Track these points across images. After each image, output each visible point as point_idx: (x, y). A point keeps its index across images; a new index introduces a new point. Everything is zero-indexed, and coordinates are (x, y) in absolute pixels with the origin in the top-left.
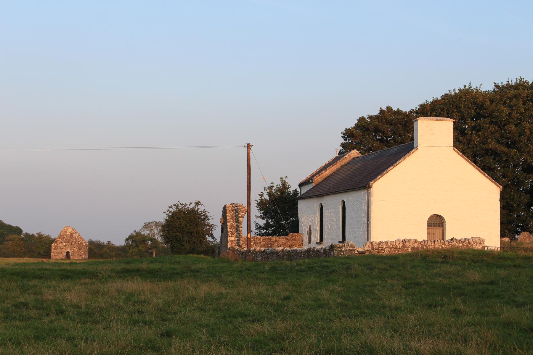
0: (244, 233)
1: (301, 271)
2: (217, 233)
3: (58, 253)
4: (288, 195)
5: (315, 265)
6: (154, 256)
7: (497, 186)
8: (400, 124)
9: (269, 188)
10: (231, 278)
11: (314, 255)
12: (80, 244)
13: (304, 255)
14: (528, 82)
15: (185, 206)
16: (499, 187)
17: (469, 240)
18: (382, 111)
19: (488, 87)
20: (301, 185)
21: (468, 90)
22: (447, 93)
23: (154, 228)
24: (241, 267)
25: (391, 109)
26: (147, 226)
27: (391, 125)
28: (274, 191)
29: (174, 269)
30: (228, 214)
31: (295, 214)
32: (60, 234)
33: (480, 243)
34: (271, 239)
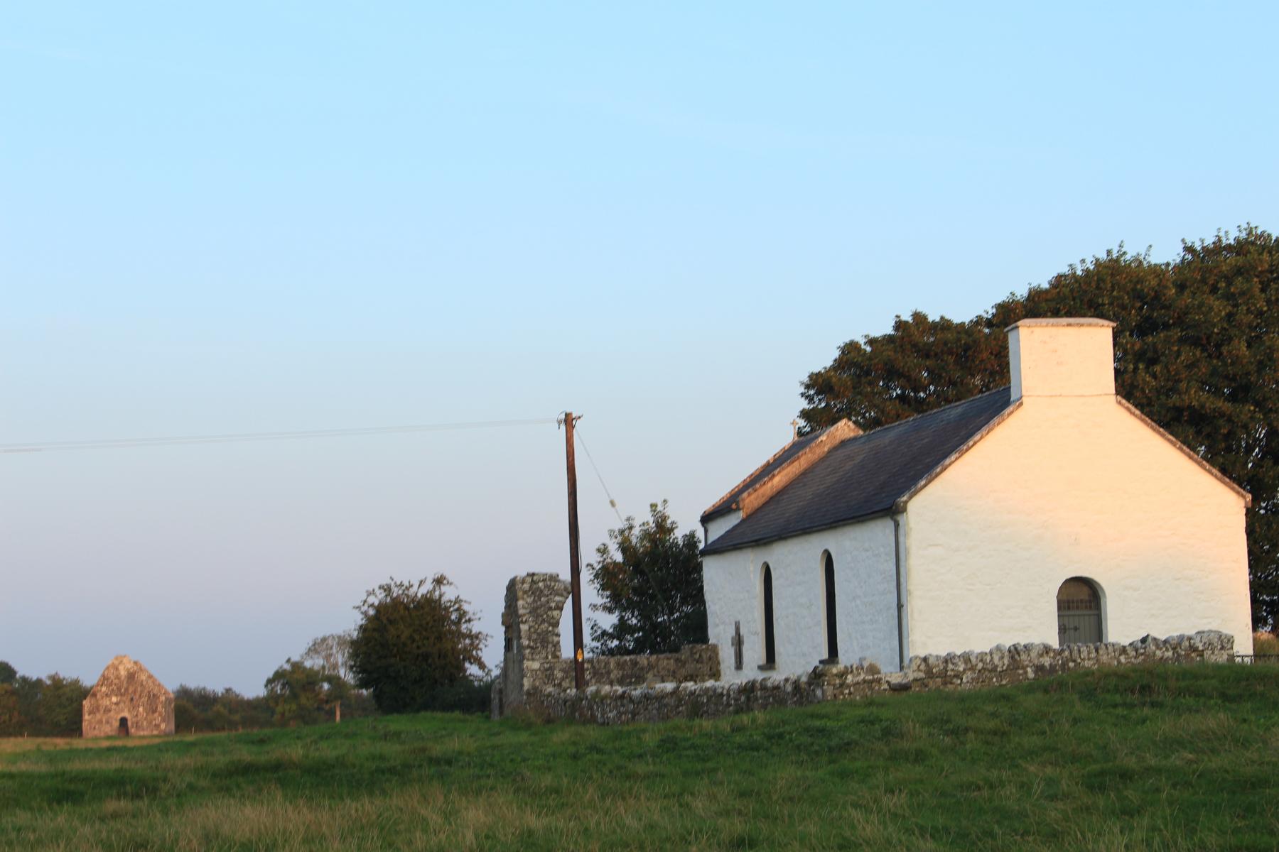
0: (567, 651)
1: (752, 749)
2: (493, 654)
3: (100, 722)
4: (671, 547)
5: (788, 728)
6: (338, 718)
7: (1238, 493)
8: (950, 353)
9: (622, 532)
10: (547, 780)
11: (766, 698)
12: (153, 698)
13: (736, 700)
14: (1269, 235)
15: (407, 589)
16: (1244, 497)
17: (1190, 639)
18: (900, 325)
19: (1166, 253)
20: (707, 519)
21: (1117, 261)
22: (1065, 270)
23: (334, 650)
24: (574, 743)
25: (925, 318)
26: (316, 647)
27: (927, 356)
28: (634, 540)
29: (382, 757)
30: (520, 603)
31: (696, 595)
32: (103, 676)
33: (1223, 648)
34: (635, 663)
